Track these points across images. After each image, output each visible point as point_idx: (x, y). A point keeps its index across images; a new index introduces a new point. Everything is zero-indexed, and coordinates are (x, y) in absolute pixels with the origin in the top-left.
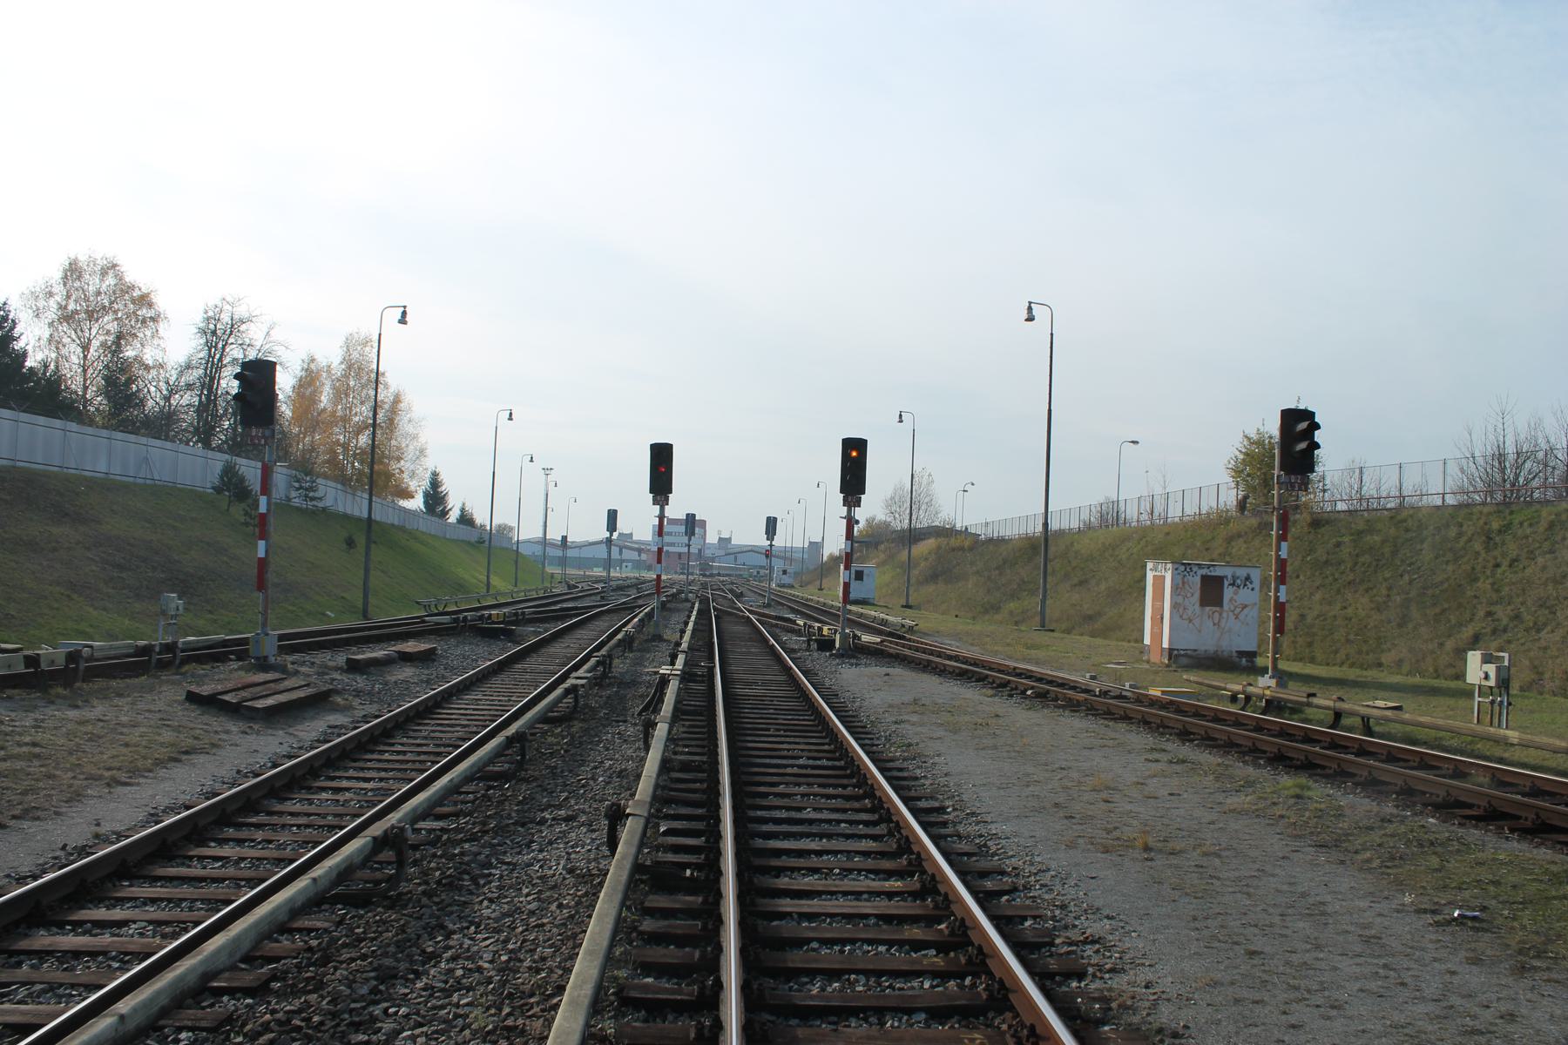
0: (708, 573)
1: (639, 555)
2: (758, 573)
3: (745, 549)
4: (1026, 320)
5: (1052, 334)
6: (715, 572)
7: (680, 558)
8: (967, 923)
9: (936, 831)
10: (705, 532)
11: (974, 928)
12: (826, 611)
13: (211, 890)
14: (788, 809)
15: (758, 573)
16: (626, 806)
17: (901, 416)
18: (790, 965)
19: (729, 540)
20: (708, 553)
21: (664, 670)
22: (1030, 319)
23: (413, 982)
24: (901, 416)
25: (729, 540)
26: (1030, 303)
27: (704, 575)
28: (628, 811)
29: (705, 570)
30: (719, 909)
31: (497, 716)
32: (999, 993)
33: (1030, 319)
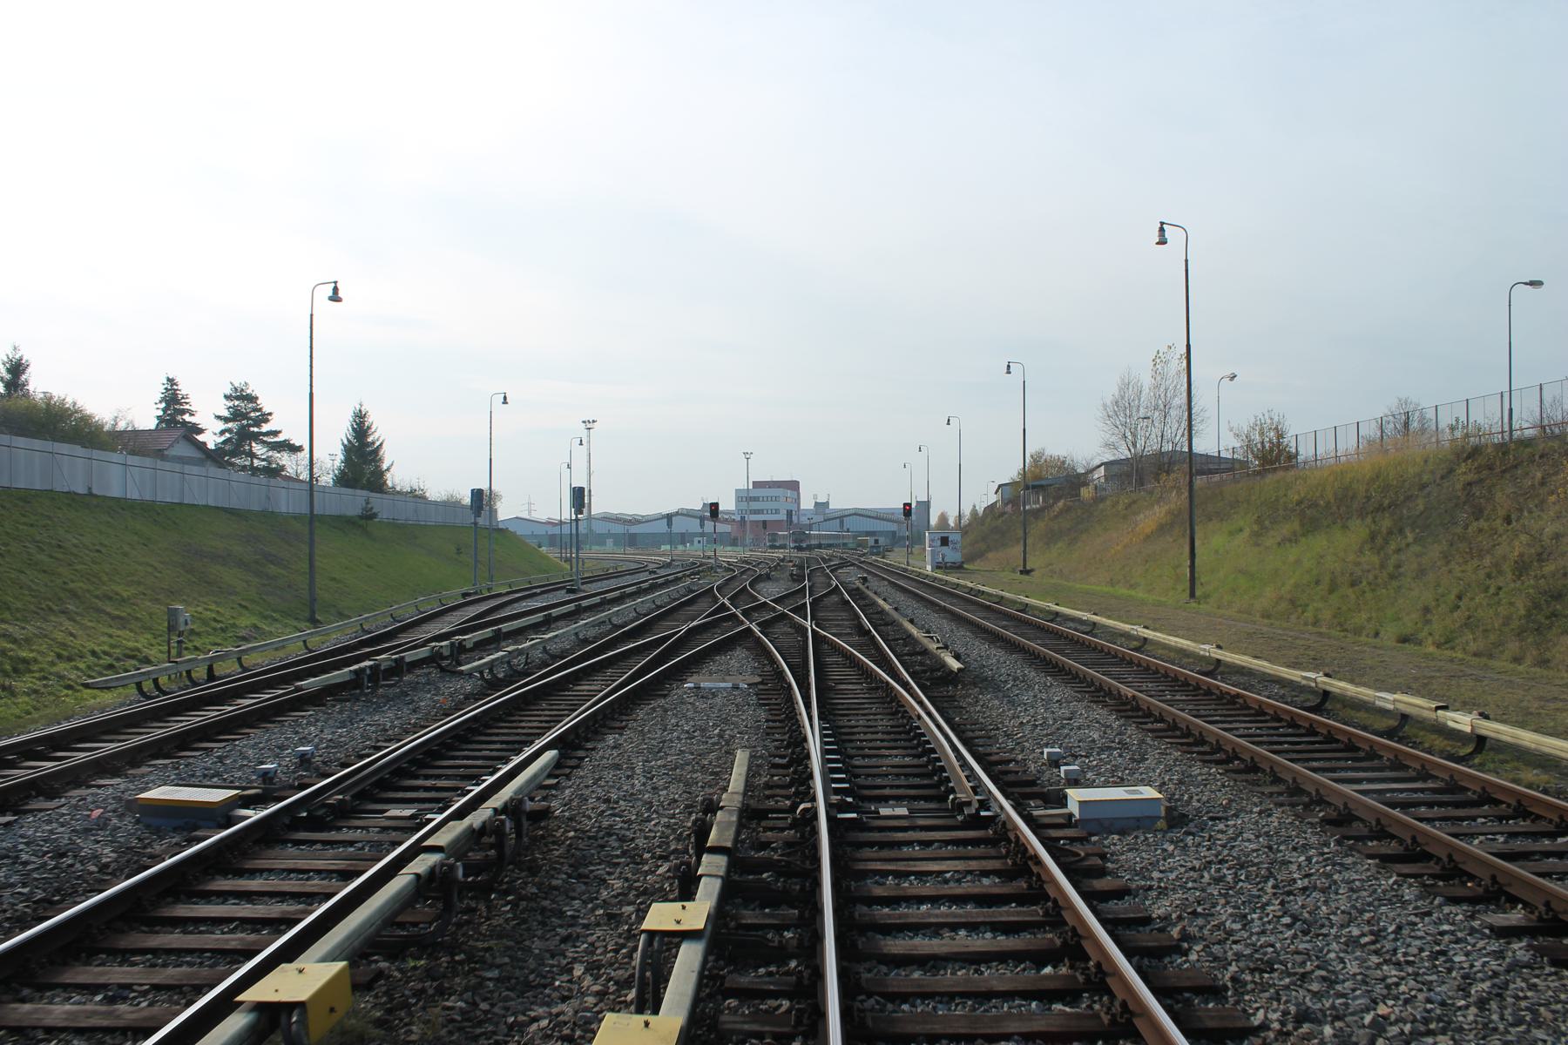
0: (804, 545)
1: (702, 525)
2: (876, 541)
3: (649, 518)
4: (1157, 243)
5: (1186, 261)
6: (813, 542)
7: (765, 528)
8: (1104, 967)
9: (1115, 907)
10: (799, 494)
11: (1067, 909)
12: (949, 593)
13: (171, 974)
14: (872, 733)
15: (876, 541)
16: (720, 800)
17: (1009, 366)
18: (890, 990)
19: (827, 504)
20: (804, 520)
21: (661, 916)
22: (1162, 242)
23: (634, 773)
24: (1009, 366)
25: (827, 504)
26: (1162, 223)
27: (800, 549)
28: (721, 804)
29: (801, 541)
30: (815, 896)
31: (545, 728)
32: (1096, 977)
33: (1162, 242)
